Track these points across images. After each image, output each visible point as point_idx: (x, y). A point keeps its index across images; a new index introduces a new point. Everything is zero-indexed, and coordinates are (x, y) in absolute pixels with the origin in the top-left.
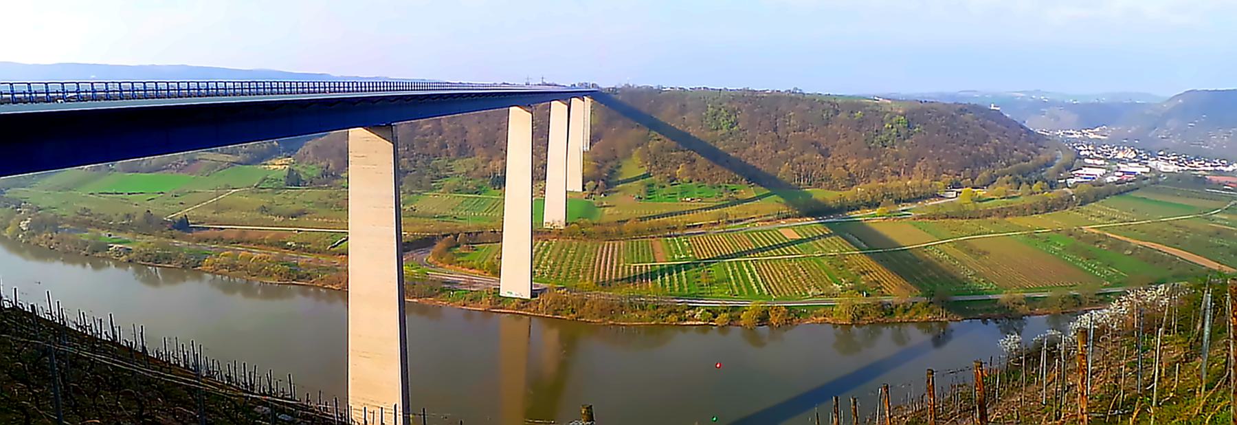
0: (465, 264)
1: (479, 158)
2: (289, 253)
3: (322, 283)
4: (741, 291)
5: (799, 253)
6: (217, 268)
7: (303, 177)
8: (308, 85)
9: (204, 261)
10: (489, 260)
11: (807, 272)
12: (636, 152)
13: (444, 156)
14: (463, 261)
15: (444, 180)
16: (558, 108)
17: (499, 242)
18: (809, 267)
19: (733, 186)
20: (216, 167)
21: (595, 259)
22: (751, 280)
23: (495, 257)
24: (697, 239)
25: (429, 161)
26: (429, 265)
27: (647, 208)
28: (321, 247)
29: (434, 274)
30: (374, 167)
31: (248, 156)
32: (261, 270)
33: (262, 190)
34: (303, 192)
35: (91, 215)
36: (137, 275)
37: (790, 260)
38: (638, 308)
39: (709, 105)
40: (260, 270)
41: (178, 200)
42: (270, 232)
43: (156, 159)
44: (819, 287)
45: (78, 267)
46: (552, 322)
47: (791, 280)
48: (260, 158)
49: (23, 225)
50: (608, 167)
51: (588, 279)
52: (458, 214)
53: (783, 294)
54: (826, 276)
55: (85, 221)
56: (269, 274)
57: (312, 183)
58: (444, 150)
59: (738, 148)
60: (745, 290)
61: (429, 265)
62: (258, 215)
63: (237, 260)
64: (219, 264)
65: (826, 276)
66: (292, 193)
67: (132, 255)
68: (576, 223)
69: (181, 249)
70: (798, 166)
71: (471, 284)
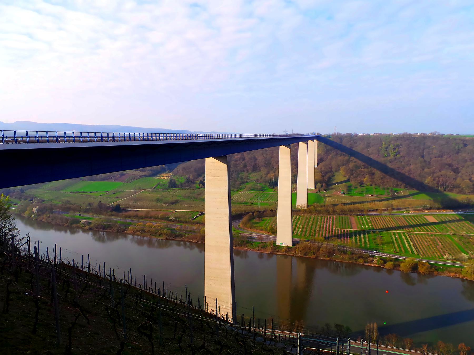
0: (258, 228)
1: (263, 171)
2: (171, 223)
3: (188, 239)
4: (400, 250)
5: (438, 232)
6: (135, 232)
7: (177, 183)
8: (188, 135)
9: (128, 228)
10: (270, 226)
11: (443, 243)
12: (342, 169)
13: (246, 172)
14: (257, 226)
15: (246, 184)
16: (302, 145)
17: (274, 216)
18: (444, 241)
19: (395, 189)
20: (134, 178)
21: (323, 225)
22: (407, 245)
23: (273, 224)
24: (375, 218)
25: (238, 174)
26: (240, 228)
27: (347, 199)
28: (187, 220)
29: (243, 234)
30: (218, 177)
31: (150, 172)
32: (157, 233)
33: (157, 190)
34: (178, 191)
35: (70, 204)
36: (93, 237)
37: (432, 235)
38: (342, 253)
39: (384, 143)
40: (156, 233)
41: (114, 196)
42: (162, 211)
43: (104, 175)
44: (451, 254)
45: (63, 233)
46: (302, 259)
47: (433, 248)
48: (156, 174)
49: (34, 210)
50: (328, 175)
51: (320, 235)
52: (253, 201)
53: (427, 255)
54: (457, 247)
55: (67, 208)
56: (161, 235)
57: (182, 186)
58: (245, 169)
59: (399, 167)
60: (403, 250)
61: (240, 228)
62: (155, 203)
63: (145, 227)
64: (135, 230)
65: (457, 247)
66: (171, 191)
67: (91, 226)
68: (313, 206)
69: (116, 222)
70: (437, 178)
71: (261, 239)
